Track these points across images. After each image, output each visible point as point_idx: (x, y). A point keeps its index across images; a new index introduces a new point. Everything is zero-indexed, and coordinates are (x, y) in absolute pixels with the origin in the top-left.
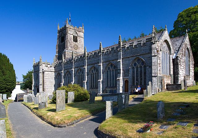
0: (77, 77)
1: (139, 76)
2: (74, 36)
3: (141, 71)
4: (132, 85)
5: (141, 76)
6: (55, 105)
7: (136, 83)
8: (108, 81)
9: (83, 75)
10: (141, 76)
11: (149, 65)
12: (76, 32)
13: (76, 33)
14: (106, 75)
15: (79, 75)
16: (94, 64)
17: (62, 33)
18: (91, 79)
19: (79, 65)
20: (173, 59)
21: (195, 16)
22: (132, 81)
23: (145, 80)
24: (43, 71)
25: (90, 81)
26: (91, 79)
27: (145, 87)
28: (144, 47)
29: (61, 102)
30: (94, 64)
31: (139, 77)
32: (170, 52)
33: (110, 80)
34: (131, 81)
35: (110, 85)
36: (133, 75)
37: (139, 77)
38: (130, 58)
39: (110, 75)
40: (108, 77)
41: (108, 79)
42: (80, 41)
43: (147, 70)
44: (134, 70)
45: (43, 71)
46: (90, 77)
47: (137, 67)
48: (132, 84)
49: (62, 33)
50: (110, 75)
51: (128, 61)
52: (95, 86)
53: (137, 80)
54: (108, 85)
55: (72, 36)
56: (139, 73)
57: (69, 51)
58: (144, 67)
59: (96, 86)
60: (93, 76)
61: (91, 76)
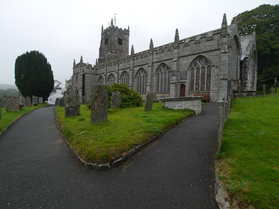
0: (122, 80)
1: (200, 79)
2: (118, 38)
3: (203, 74)
4: (190, 90)
5: (203, 79)
6: (262, 95)
7: (196, 88)
8: (158, 85)
9: (129, 78)
10: (203, 79)
11: (215, 65)
12: (121, 34)
13: (121, 35)
14: (157, 77)
15: (123, 78)
16: (142, 65)
17: (106, 34)
18: (138, 83)
19: (124, 67)
20: (240, 61)
21: (135, 96)
22: (190, 85)
23: (208, 85)
24: (84, 73)
25: (137, 85)
26: (138, 83)
27: (208, 93)
28: (209, 42)
29: (100, 106)
30: (142, 65)
31: (200, 81)
32: (238, 51)
33: (161, 85)
34: (189, 85)
35: (161, 90)
36: (192, 77)
37: (200, 81)
38: (190, 57)
39: (162, 78)
40: (158, 80)
41: (158, 83)
42: (125, 44)
43: (212, 71)
44: (194, 72)
45: (84, 73)
46: (137, 81)
47: (198, 68)
48: (190, 89)
49: (106, 34)
50: (162, 78)
51: (186, 61)
52: (142, 91)
53: (197, 84)
54: (158, 90)
55: (117, 38)
56: (200, 75)
57: (113, 54)
58: (207, 68)
59: (143, 91)
60: (141, 80)
61: (138, 80)
